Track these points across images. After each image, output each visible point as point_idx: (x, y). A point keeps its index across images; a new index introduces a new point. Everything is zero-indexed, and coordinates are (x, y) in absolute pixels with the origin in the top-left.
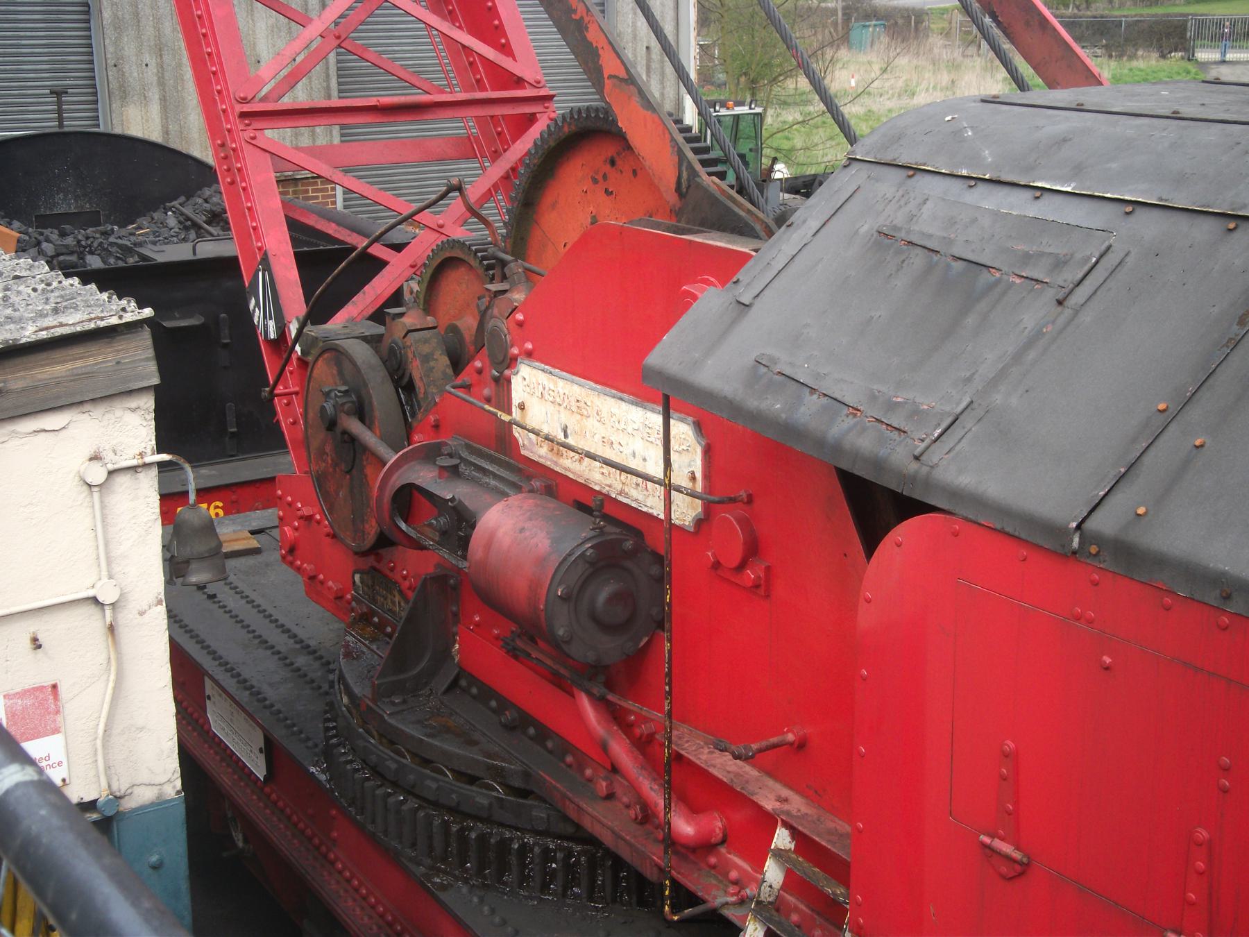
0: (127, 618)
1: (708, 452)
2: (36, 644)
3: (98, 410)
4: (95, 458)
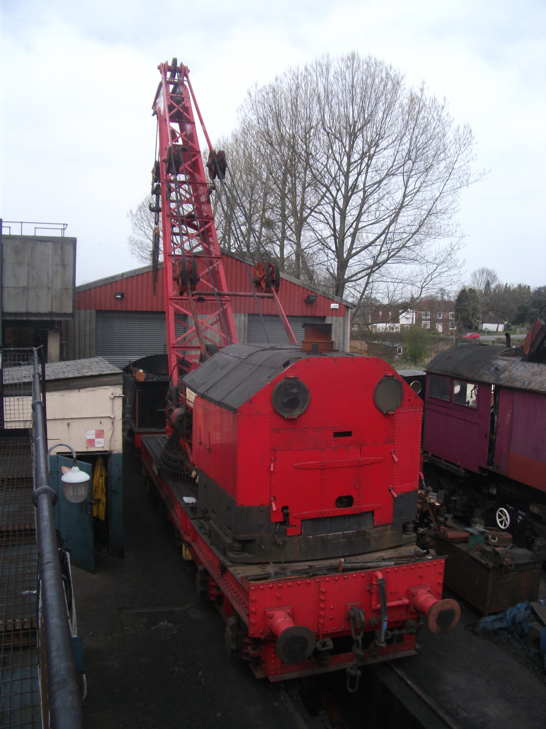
0: (115, 421)
1: (333, 642)
2: (101, 423)
3: (113, 387)
4: (112, 394)
